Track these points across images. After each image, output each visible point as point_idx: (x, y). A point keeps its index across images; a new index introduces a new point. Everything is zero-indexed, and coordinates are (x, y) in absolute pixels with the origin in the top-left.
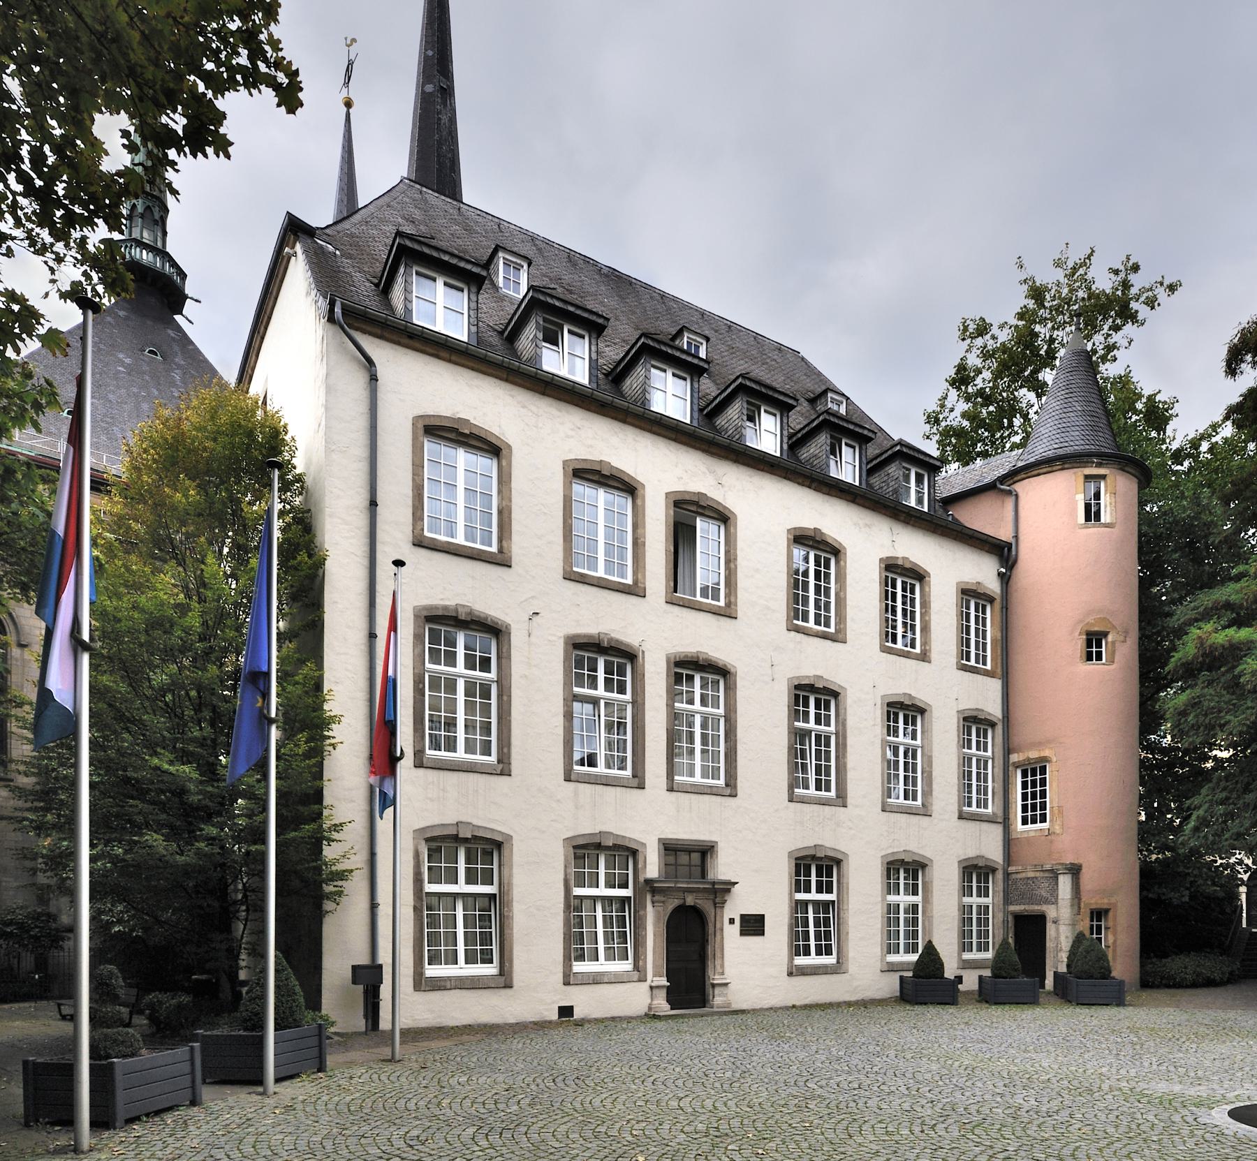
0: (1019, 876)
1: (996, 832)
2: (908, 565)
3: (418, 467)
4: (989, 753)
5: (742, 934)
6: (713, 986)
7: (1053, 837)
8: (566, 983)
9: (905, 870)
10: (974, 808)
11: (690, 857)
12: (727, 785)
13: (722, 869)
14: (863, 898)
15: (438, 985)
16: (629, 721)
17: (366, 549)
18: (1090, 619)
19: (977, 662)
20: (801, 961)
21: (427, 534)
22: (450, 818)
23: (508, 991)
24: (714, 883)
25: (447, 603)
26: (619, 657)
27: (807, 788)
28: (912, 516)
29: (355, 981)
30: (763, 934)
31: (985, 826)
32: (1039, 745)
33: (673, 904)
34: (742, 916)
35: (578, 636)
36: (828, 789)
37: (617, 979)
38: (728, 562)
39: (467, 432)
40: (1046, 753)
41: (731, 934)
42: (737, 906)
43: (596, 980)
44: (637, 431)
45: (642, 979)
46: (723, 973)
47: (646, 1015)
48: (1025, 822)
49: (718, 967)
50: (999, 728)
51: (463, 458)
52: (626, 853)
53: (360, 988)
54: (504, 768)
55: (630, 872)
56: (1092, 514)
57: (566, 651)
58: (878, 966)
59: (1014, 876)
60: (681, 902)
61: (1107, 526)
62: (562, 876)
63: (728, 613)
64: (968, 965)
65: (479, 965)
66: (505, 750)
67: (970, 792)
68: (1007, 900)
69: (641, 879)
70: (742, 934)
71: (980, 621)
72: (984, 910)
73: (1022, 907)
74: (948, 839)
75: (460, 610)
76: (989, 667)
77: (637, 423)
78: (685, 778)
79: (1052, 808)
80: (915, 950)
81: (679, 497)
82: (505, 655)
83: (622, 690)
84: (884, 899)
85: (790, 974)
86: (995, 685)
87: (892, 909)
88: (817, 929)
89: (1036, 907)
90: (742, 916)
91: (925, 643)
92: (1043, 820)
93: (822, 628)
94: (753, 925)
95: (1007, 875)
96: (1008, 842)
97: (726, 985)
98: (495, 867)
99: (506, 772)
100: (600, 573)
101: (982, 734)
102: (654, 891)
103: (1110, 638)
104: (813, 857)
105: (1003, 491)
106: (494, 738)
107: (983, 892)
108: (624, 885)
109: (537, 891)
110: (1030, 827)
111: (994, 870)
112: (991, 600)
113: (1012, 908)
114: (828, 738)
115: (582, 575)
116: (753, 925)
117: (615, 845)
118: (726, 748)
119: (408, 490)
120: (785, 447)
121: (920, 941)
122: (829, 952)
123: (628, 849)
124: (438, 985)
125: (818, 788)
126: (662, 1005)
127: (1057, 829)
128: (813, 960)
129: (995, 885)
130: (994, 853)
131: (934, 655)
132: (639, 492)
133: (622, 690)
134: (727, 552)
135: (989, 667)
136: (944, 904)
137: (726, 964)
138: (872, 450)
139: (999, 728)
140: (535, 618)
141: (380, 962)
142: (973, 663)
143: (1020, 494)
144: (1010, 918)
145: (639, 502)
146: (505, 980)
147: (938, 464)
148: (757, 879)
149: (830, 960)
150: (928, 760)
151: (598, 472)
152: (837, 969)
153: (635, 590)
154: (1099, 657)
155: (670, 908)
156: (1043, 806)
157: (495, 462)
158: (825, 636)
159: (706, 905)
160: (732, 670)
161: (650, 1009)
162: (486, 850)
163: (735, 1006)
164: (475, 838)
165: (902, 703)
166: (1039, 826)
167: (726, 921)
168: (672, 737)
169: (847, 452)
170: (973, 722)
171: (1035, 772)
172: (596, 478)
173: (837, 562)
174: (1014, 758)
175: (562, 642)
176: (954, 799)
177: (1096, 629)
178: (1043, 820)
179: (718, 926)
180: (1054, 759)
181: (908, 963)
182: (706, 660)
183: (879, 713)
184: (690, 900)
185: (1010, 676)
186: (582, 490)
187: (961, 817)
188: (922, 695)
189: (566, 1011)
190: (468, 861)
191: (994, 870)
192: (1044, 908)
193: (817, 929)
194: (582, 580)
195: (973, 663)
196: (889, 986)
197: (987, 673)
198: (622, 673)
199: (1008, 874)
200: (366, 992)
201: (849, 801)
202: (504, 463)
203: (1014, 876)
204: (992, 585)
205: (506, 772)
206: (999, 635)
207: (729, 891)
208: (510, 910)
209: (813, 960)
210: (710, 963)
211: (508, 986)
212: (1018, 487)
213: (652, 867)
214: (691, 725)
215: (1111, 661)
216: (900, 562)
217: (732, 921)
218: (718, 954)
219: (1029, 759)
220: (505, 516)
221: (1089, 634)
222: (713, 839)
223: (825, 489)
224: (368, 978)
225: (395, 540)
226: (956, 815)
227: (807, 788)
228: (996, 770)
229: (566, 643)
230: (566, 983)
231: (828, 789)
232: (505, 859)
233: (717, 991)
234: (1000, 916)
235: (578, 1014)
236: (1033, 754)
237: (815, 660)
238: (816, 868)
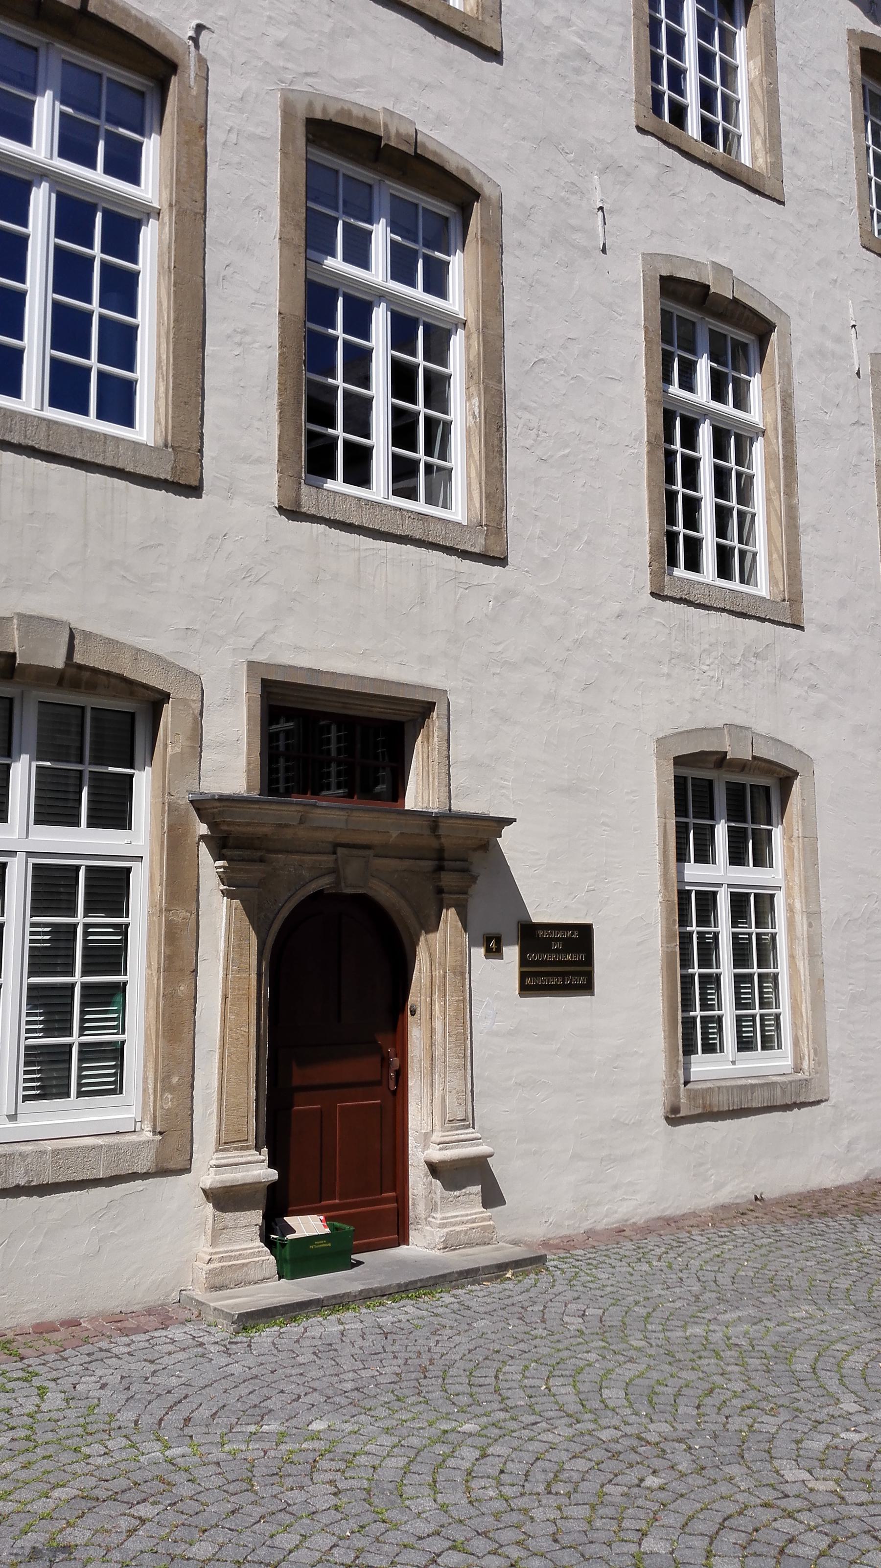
30: (586, 987)
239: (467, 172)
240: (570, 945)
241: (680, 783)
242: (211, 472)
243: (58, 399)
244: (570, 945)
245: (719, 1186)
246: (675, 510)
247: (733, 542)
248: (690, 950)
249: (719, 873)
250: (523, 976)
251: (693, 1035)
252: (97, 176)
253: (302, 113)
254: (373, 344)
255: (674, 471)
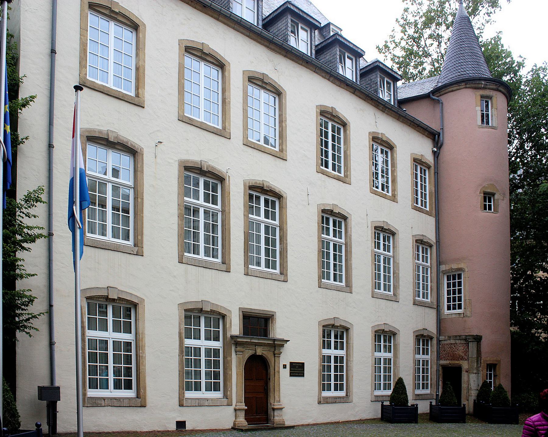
0: (446, 342)
1: (432, 314)
2: (384, 139)
3: (83, 30)
4: (429, 264)
5: (291, 376)
6: (274, 409)
7: (466, 318)
8: (181, 405)
9: (384, 336)
10: (421, 298)
11: (257, 323)
12: (281, 274)
13: (279, 331)
14: (362, 353)
15: (96, 403)
16: (219, 224)
17: (47, 84)
18: (485, 184)
19: (422, 205)
20: (326, 394)
21: (88, 77)
22: (103, 284)
23: (142, 409)
24: (274, 340)
25: (102, 128)
26: (215, 180)
27: (104, 234)
28: (387, 107)
29: (41, 398)
30: (303, 376)
31: (427, 310)
32: (458, 260)
33: (249, 353)
34: (291, 363)
35: (188, 161)
36: (274, 268)
37: (213, 404)
38: (281, 122)
39: (117, 11)
40: (462, 266)
41: (284, 373)
42: (288, 356)
43: (200, 403)
44: (226, 27)
45: (229, 404)
46: (279, 401)
47: (232, 428)
48: (449, 309)
49: (277, 397)
50: (434, 248)
51: (112, 27)
52: (217, 317)
53: (45, 403)
54: (138, 250)
55: (221, 330)
56: (485, 118)
57: (179, 171)
58: (369, 398)
59: (443, 342)
60: (253, 352)
61: (493, 128)
62: (177, 331)
63: (281, 156)
64: (419, 397)
65: (123, 390)
66: (139, 237)
67: (419, 288)
68: (439, 358)
69: (229, 335)
70: (291, 376)
71: (423, 179)
72: (425, 362)
73: (447, 362)
74: (409, 318)
75: (110, 134)
76: (428, 209)
77: (226, 21)
78: (192, 200)
79: (465, 300)
80: (389, 388)
81: (251, 75)
82: (139, 169)
83: (215, 202)
84: (373, 355)
85: (319, 403)
86: (431, 221)
87: (378, 361)
88: (334, 375)
89: (456, 362)
90: (291, 363)
91: (394, 190)
92: (460, 307)
93: (336, 173)
94: (297, 369)
95: (439, 341)
96: (440, 321)
97: (281, 409)
98: (133, 320)
99: (140, 254)
100: (202, 119)
101: (425, 251)
102: (237, 344)
103: (496, 197)
104: (333, 326)
105: (434, 99)
106: (131, 228)
107: (425, 352)
108: (217, 339)
109: (161, 342)
110: (452, 311)
111: (431, 338)
112: (429, 167)
113: (443, 362)
114: (340, 247)
115: (190, 119)
116: (297, 369)
117: (211, 311)
118: (281, 248)
119: (77, 46)
120: (314, 52)
121: (392, 382)
122: (341, 389)
123: (220, 314)
124: (96, 403)
125: (267, 266)
126: (242, 420)
127: (468, 313)
128: (332, 393)
129: (432, 347)
130: (432, 329)
131: (399, 198)
132: (227, 68)
133: (215, 202)
134: (280, 115)
135: (428, 209)
136: (406, 361)
137: (281, 395)
138: (362, 64)
139: (434, 248)
140: (160, 145)
141: (57, 384)
142: (419, 205)
143: (444, 103)
144: (440, 368)
145: (226, 74)
146: (140, 401)
147: (399, 77)
148: (298, 338)
149: (342, 394)
150: (396, 264)
151: (201, 51)
152: (346, 399)
153: (223, 133)
154: (490, 209)
155: (247, 356)
156: (460, 300)
157: (134, 33)
158: (339, 179)
159: (268, 355)
160: (284, 195)
161: (234, 424)
162: (127, 309)
163: (287, 424)
164: (120, 299)
165: (382, 228)
166: (458, 311)
167: (281, 366)
168: (248, 237)
169: (348, 62)
170: (421, 243)
171: (455, 277)
172: (199, 54)
173: (345, 131)
174: (443, 268)
175: (177, 164)
176: (369, 285)
177: (489, 191)
178: (460, 307)
179: (276, 369)
180: (467, 270)
181: (386, 396)
182: (268, 187)
183: (370, 232)
184: (260, 351)
185: (440, 215)
186: (190, 62)
187: (414, 304)
188: (394, 224)
189: (181, 425)
190: (114, 315)
191: (431, 338)
192: (461, 362)
193: (334, 375)
194: (190, 122)
195: (419, 205)
196: (375, 411)
197: (427, 213)
198: (215, 190)
199: (440, 341)
200: (48, 406)
201: (354, 289)
202: (141, 35)
203: (443, 342)
204: (429, 158)
205: (140, 254)
206: (433, 189)
207: (282, 346)
208: (144, 353)
209: (332, 393)
210: (271, 395)
211: (143, 406)
212: (443, 99)
213: (235, 327)
214: (259, 230)
215: (496, 211)
216: (380, 136)
217: (285, 367)
218: (276, 389)
219: (452, 269)
220: (139, 71)
221: (485, 193)
222: (273, 309)
223: (338, 83)
224: (50, 395)
225: (67, 77)
226: (412, 303)
227: (104, 234)
228: (433, 275)
229: (179, 166)
230: (181, 405)
231: (274, 268)
232: (140, 316)
233: (276, 413)
234: (435, 367)
235: (188, 427)
236: (455, 266)
237: (333, 194)
238: (335, 333)
239: (280, 192)
240: (300, 367)
241: (324, 331)
242: (144, 254)
243: (114, 236)
244: (300, 367)
245: (329, 418)
246: (323, 265)
247: (387, 243)
248: (325, 368)
249: (332, 352)
250: (290, 373)
251: (325, 387)
252: (210, 205)
253: (248, 185)
254: (200, 189)
255: (323, 254)
